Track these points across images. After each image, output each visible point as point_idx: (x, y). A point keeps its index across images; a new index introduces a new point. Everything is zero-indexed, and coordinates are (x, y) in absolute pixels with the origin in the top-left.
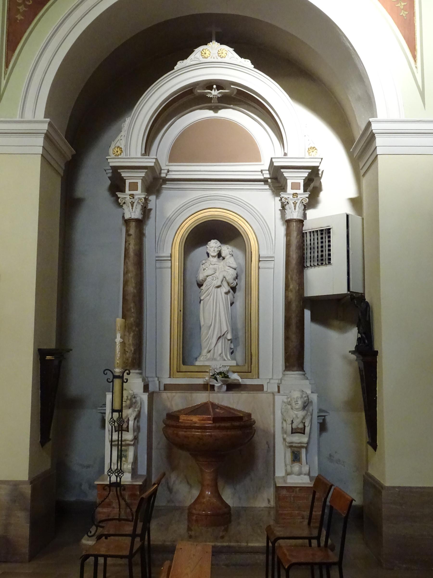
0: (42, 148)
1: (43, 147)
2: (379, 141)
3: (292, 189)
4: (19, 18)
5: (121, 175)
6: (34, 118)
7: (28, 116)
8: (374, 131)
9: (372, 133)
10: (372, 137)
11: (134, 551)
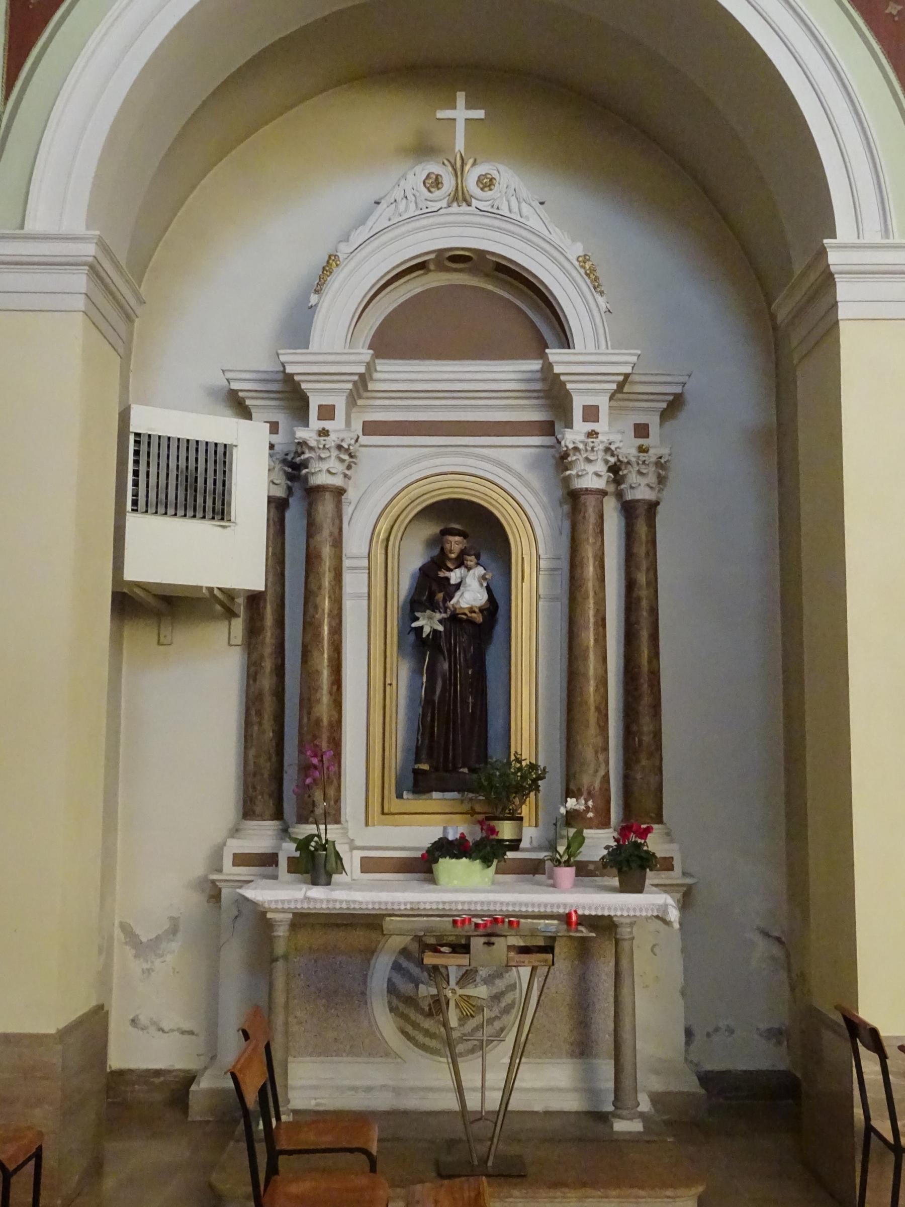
2: (844, 290)
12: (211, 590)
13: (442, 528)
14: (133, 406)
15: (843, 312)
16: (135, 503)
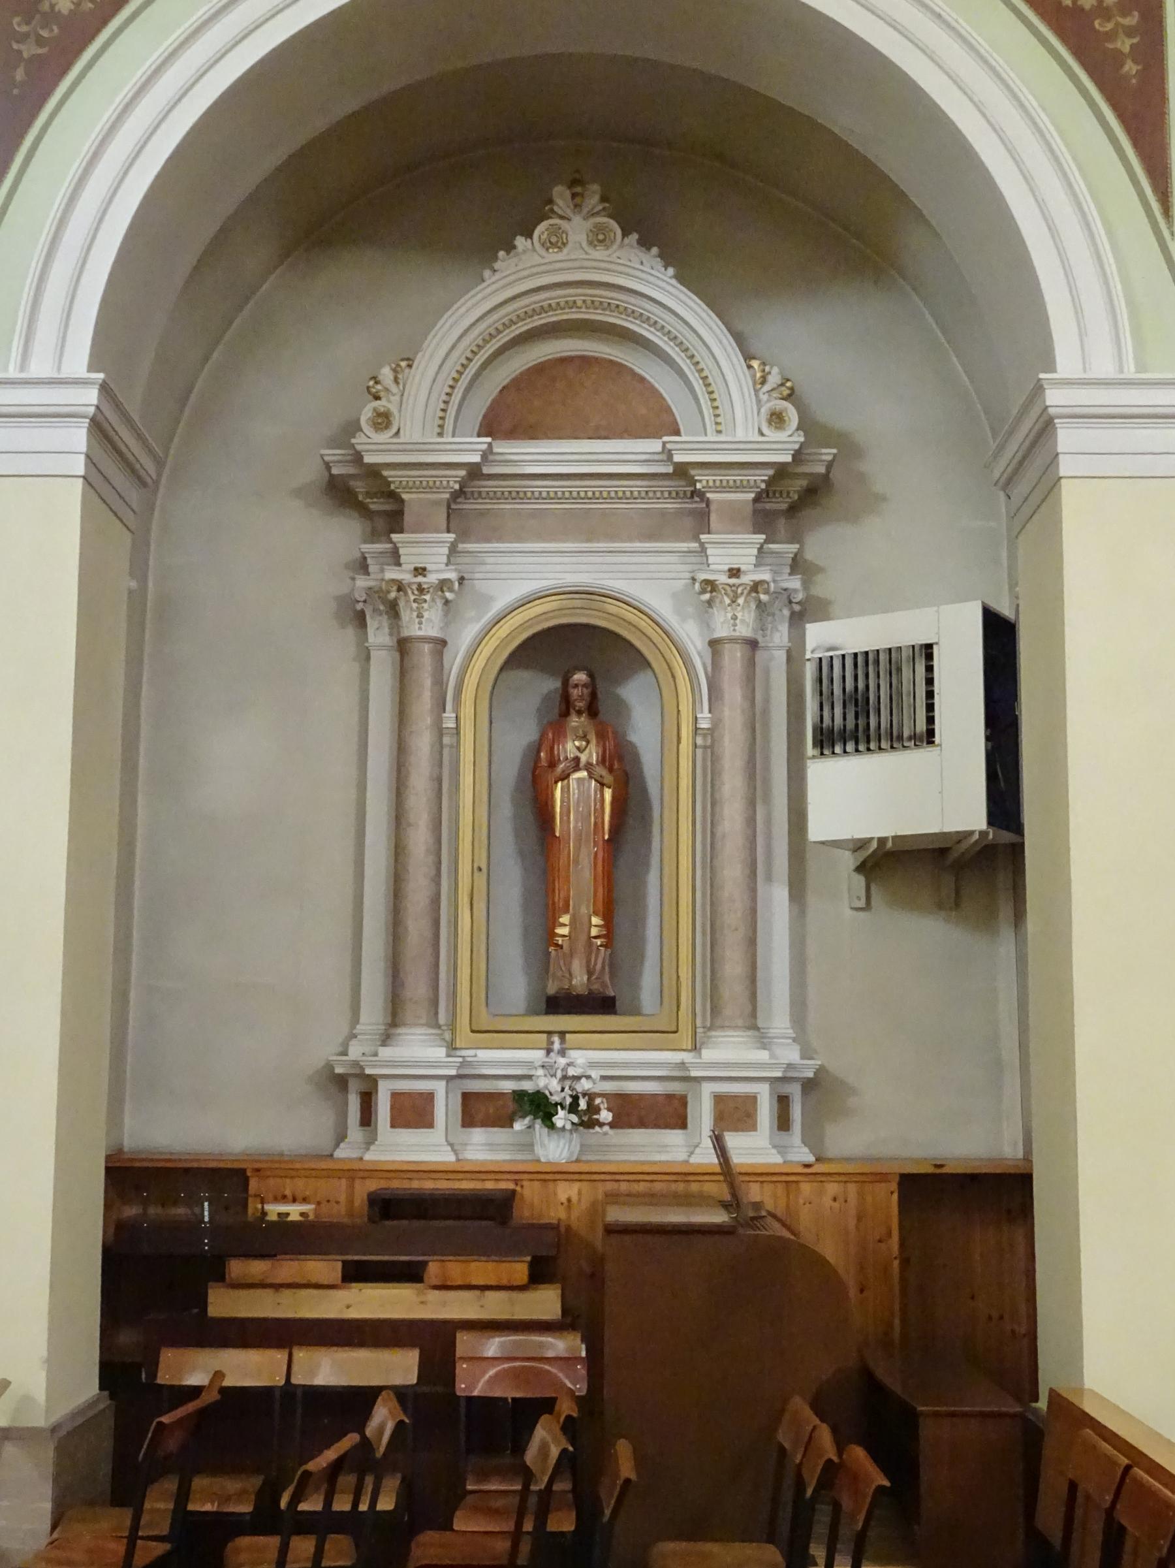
0: (82, 457)
1: (88, 456)
2: (1066, 438)
3: (393, 1126)
5: (362, 457)
6: (59, 369)
7: (39, 368)
9: (1045, 415)
10: (1046, 428)
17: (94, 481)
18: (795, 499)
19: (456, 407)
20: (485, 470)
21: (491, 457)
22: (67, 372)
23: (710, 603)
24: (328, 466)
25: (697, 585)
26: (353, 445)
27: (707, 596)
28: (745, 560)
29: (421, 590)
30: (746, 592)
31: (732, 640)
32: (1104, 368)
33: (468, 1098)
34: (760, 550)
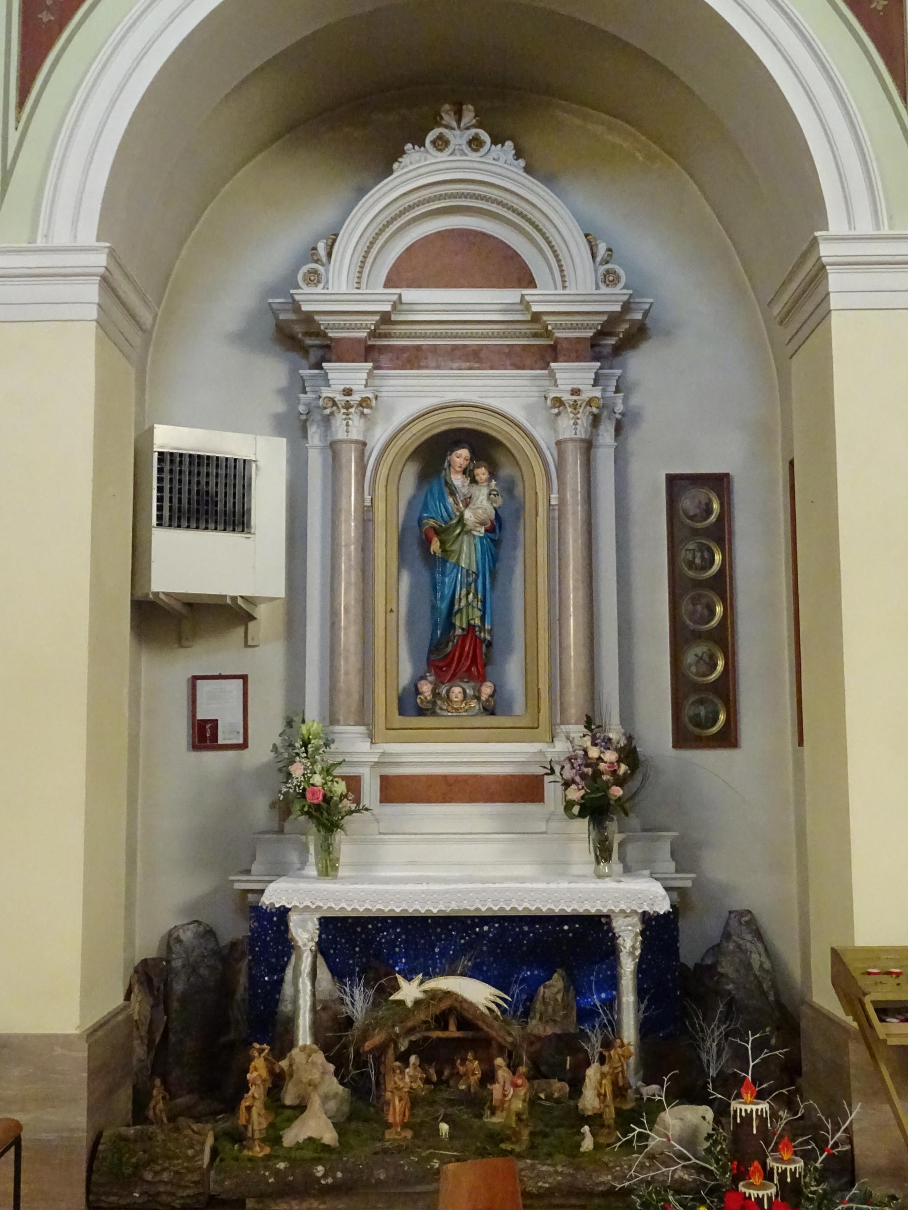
1: (99, 305)
2: (835, 280)
4: (45, 20)
5: (300, 307)
7: (62, 238)
8: (824, 260)
11: (13, 1149)
12: (234, 599)
13: (356, 1024)
14: (156, 425)
15: (835, 301)
16: (160, 518)
17: (103, 324)
18: (615, 339)
19: (369, 268)
20: (393, 318)
21: (399, 307)
22: (79, 243)
23: (558, 414)
24: (275, 313)
25: (549, 402)
26: (292, 295)
27: (556, 410)
28: (359, 382)
29: (348, 406)
30: (583, 405)
31: (572, 440)
32: (865, 226)
33: (384, 779)
34: (596, 374)
